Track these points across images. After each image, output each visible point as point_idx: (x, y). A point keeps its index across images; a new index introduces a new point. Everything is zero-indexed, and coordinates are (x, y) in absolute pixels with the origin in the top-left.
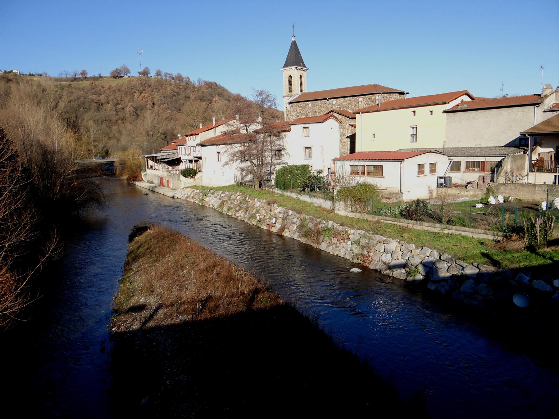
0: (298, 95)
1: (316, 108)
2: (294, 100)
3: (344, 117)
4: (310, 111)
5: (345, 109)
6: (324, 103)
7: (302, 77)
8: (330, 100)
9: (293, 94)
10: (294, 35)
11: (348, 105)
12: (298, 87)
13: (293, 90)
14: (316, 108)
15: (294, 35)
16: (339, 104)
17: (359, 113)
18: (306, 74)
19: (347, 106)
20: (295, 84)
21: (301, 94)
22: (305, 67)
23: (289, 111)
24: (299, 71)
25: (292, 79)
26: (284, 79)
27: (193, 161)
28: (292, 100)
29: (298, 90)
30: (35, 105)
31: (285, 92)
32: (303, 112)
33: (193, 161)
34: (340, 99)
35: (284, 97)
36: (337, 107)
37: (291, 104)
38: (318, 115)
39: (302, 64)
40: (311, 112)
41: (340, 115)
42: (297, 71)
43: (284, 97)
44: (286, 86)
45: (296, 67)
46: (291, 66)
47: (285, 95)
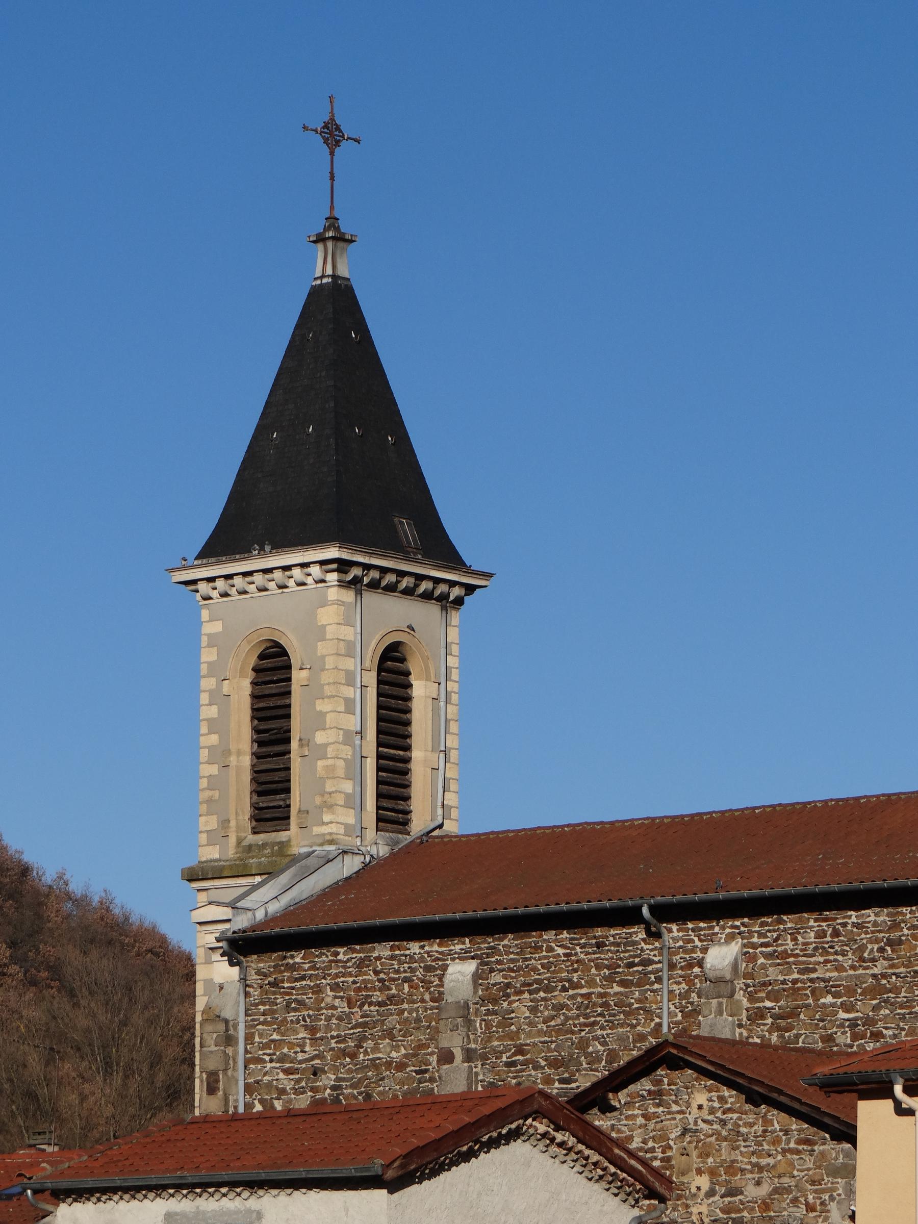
0: (352, 865)
1: (521, 1007)
2: (287, 914)
3: (795, 1125)
4: (454, 1042)
5: (843, 1038)
6: (606, 956)
7: (414, 666)
8: (673, 933)
9: (298, 849)
10: (332, 222)
11: (875, 990)
12: (355, 773)
13: (296, 799)
14: (521, 1007)
15: (332, 222)
16: (774, 974)
17: (883, 1091)
18: (454, 634)
19: (864, 1008)
20: (320, 738)
21: (383, 851)
22: (452, 559)
23: (229, 1040)
24: (372, 599)
25: (295, 687)
26: (207, 683)
27: (47, 1132)
28: (274, 908)
29: (355, 803)
30: (829, 1214)
31: (209, 823)
32: (387, 1051)
33: (47, 1132)
34: (789, 921)
35: (193, 876)
36: (757, 1015)
37: (255, 963)
38: (303, 1102)
39: (406, 528)
40: (469, 1056)
41: (754, 1099)
42: (349, 596)
43: (193, 876)
44: (221, 755)
45: (332, 552)
46: (282, 543)
47: (211, 853)
